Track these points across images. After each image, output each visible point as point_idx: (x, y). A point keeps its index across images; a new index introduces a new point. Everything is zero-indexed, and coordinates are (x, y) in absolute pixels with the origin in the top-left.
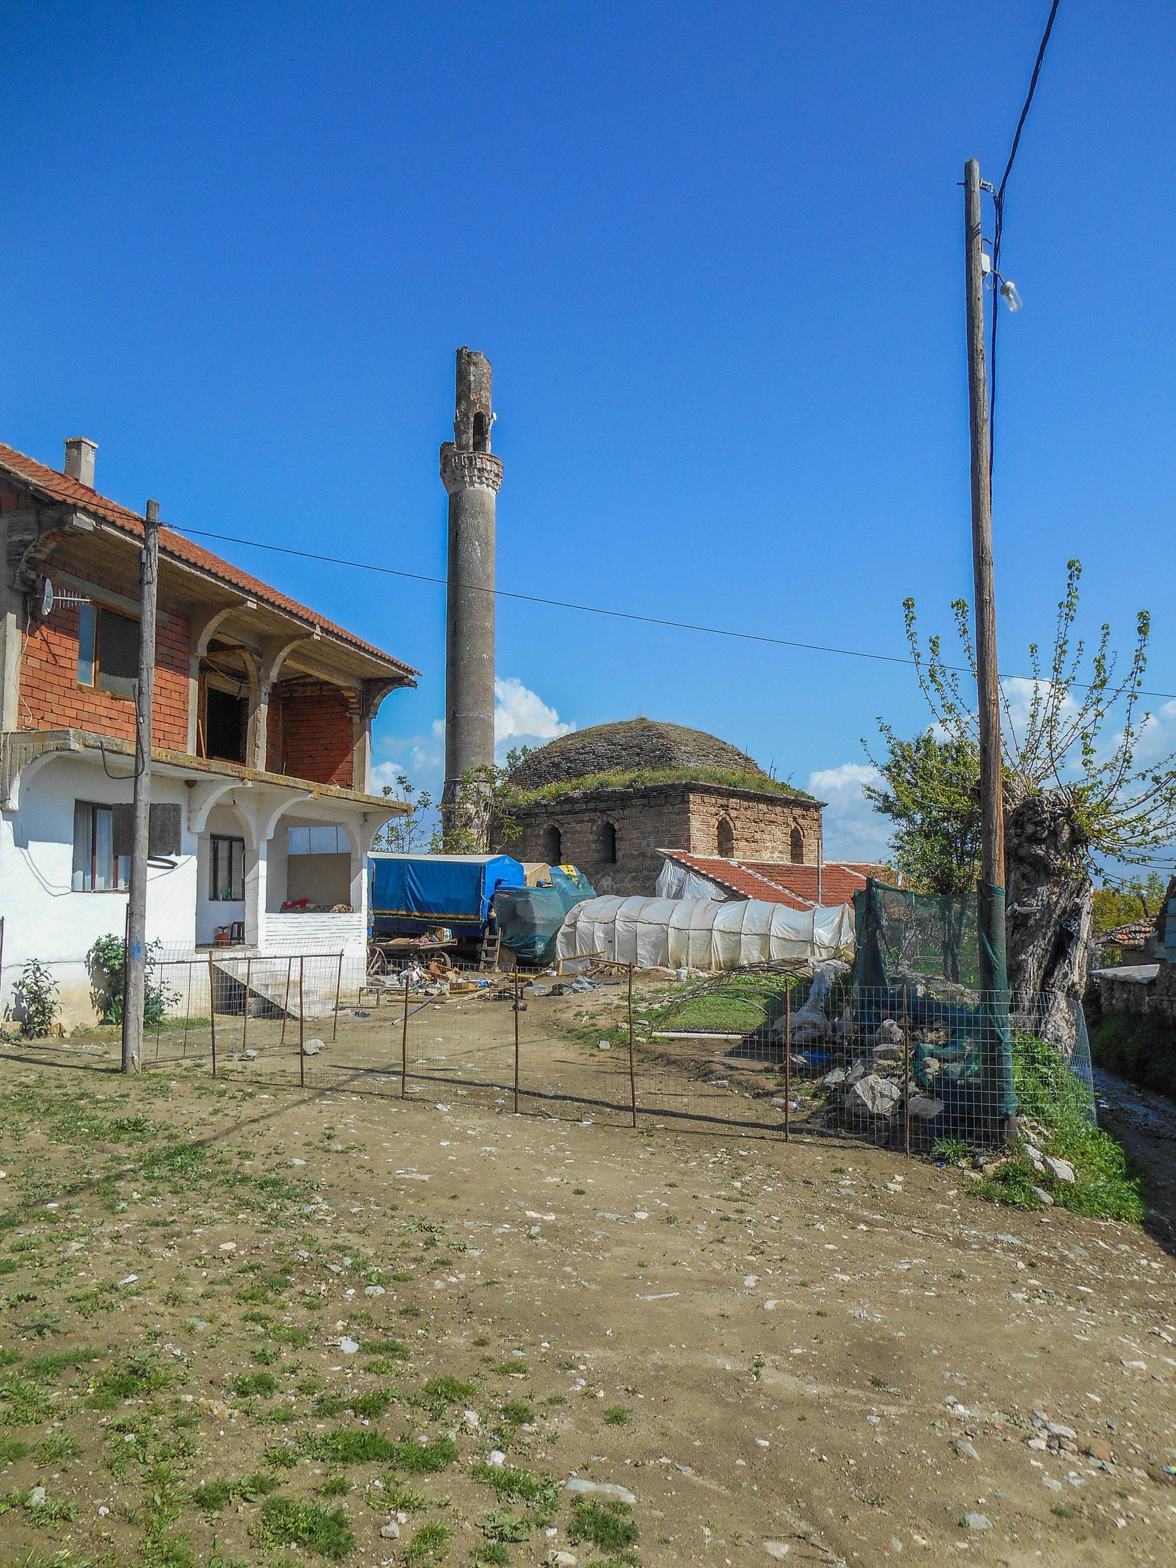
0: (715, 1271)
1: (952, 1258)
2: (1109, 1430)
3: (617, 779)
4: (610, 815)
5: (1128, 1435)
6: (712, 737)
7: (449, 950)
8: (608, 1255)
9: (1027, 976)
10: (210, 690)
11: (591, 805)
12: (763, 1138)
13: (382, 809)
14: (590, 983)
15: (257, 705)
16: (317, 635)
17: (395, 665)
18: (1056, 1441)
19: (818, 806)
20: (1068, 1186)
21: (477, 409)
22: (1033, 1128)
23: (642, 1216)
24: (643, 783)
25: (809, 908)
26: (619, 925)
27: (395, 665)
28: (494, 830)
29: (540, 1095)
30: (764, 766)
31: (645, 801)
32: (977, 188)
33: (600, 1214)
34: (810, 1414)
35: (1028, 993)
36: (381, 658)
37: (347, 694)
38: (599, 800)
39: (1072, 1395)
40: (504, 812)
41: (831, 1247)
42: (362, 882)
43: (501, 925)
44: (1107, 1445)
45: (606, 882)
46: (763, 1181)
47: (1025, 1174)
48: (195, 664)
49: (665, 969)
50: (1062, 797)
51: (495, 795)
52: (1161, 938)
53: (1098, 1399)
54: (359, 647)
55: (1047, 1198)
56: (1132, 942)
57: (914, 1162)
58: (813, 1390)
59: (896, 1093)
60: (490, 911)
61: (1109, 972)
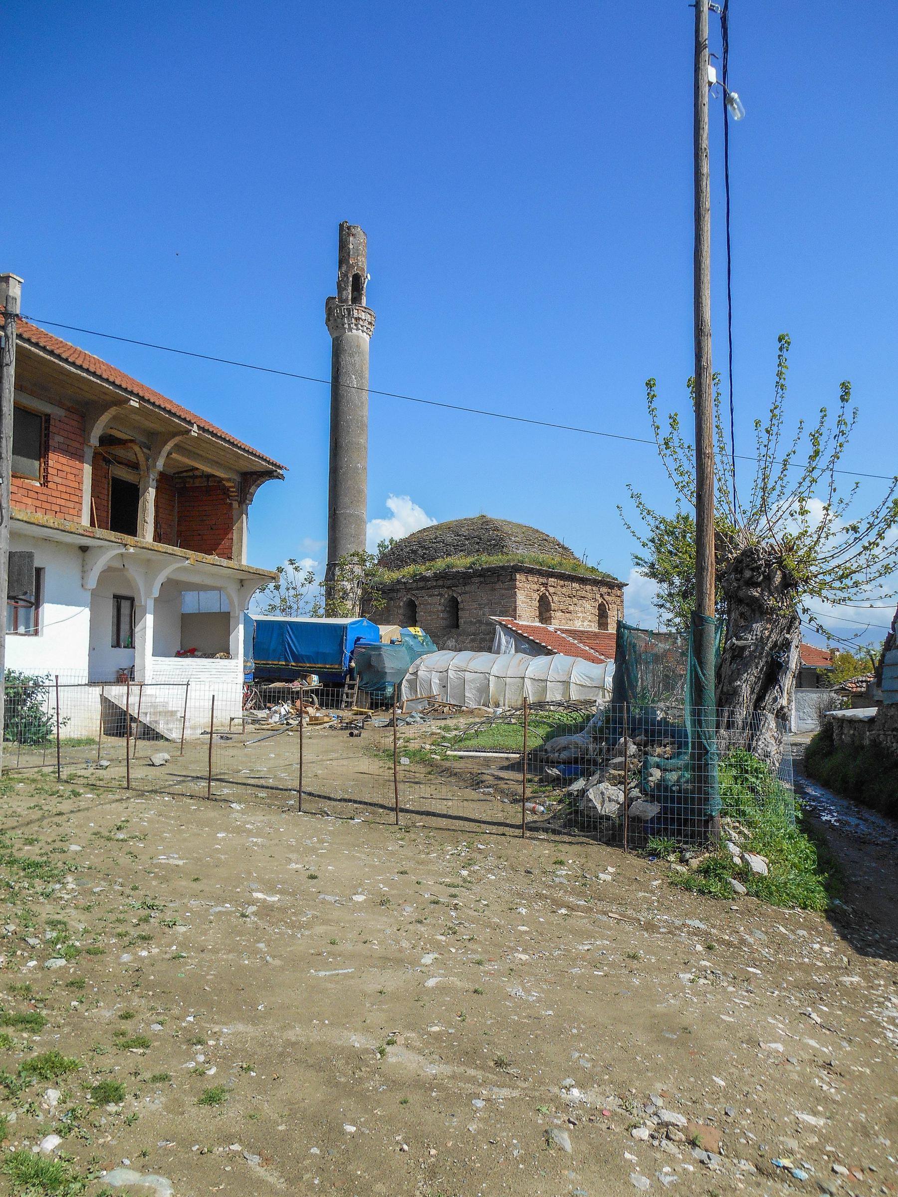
0: (401, 951)
1: (635, 940)
2: (724, 1117)
3: (460, 562)
4: (453, 591)
5: (744, 1122)
6: (537, 531)
7: (316, 692)
8: (307, 933)
9: (741, 699)
10: (114, 479)
11: (440, 583)
12: (504, 835)
13: (252, 576)
14: (421, 718)
15: (146, 490)
16: (195, 431)
17: (265, 460)
18: (664, 1129)
19: (621, 586)
20: (762, 879)
21: (355, 271)
22: (734, 828)
23: (360, 898)
24: (480, 565)
25: (602, 661)
26: (451, 674)
27: (265, 460)
28: (365, 602)
29: (330, 799)
30: (578, 554)
31: (482, 579)
32: (705, 8)
33: (322, 896)
34: (415, 1098)
35: (742, 714)
36: (252, 454)
37: (228, 484)
38: (446, 578)
39: (697, 1078)
40: (372, 588)
41: (525, 928)
42: (239, 637)
43: (359, 673)
44: (718, 1133)
45: (451, 643)
46: (490, 871)
47: (724, 868)
48: (89, 453)
49: (486, 708)
50: (776, 548)
51: (367, 575)
52: (879, 684)
53: (722, 1083)
54: (233, 444)
55: (740, 888)
56: (859, 689)
57: (629, 856)
58: (433, 1070)
59: (621, 799)
60: (350, 662)
61: (839, 713)
